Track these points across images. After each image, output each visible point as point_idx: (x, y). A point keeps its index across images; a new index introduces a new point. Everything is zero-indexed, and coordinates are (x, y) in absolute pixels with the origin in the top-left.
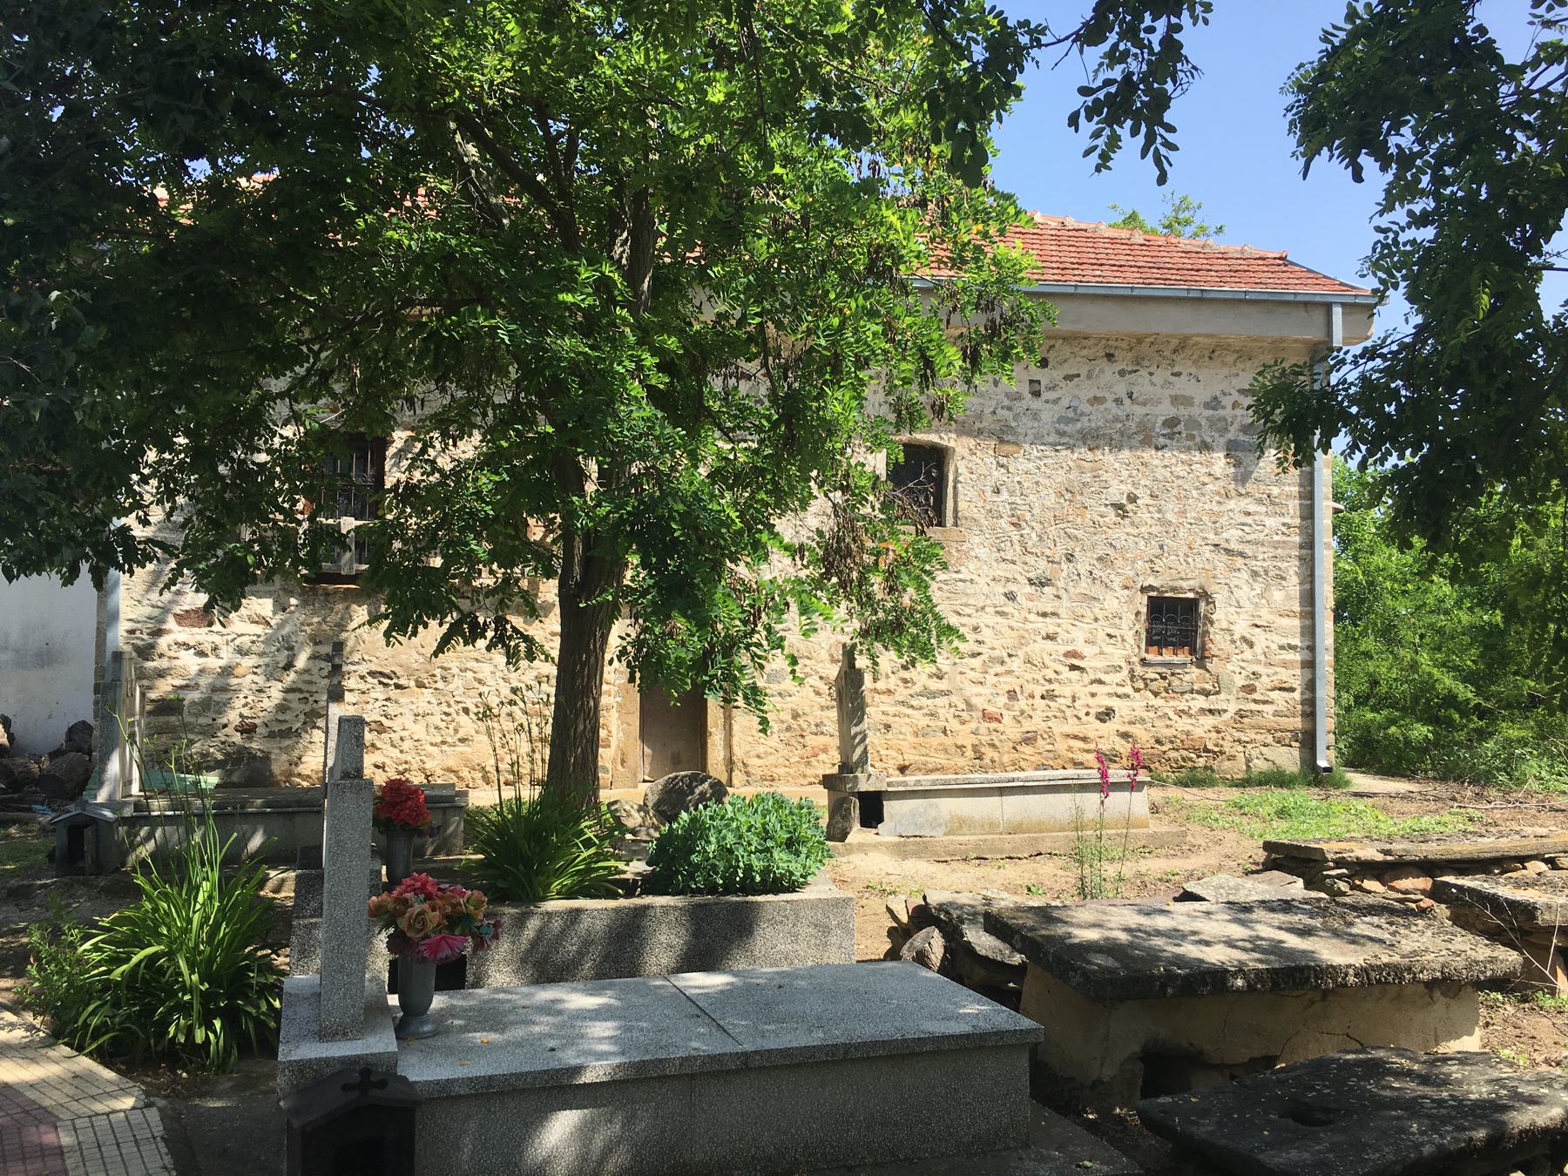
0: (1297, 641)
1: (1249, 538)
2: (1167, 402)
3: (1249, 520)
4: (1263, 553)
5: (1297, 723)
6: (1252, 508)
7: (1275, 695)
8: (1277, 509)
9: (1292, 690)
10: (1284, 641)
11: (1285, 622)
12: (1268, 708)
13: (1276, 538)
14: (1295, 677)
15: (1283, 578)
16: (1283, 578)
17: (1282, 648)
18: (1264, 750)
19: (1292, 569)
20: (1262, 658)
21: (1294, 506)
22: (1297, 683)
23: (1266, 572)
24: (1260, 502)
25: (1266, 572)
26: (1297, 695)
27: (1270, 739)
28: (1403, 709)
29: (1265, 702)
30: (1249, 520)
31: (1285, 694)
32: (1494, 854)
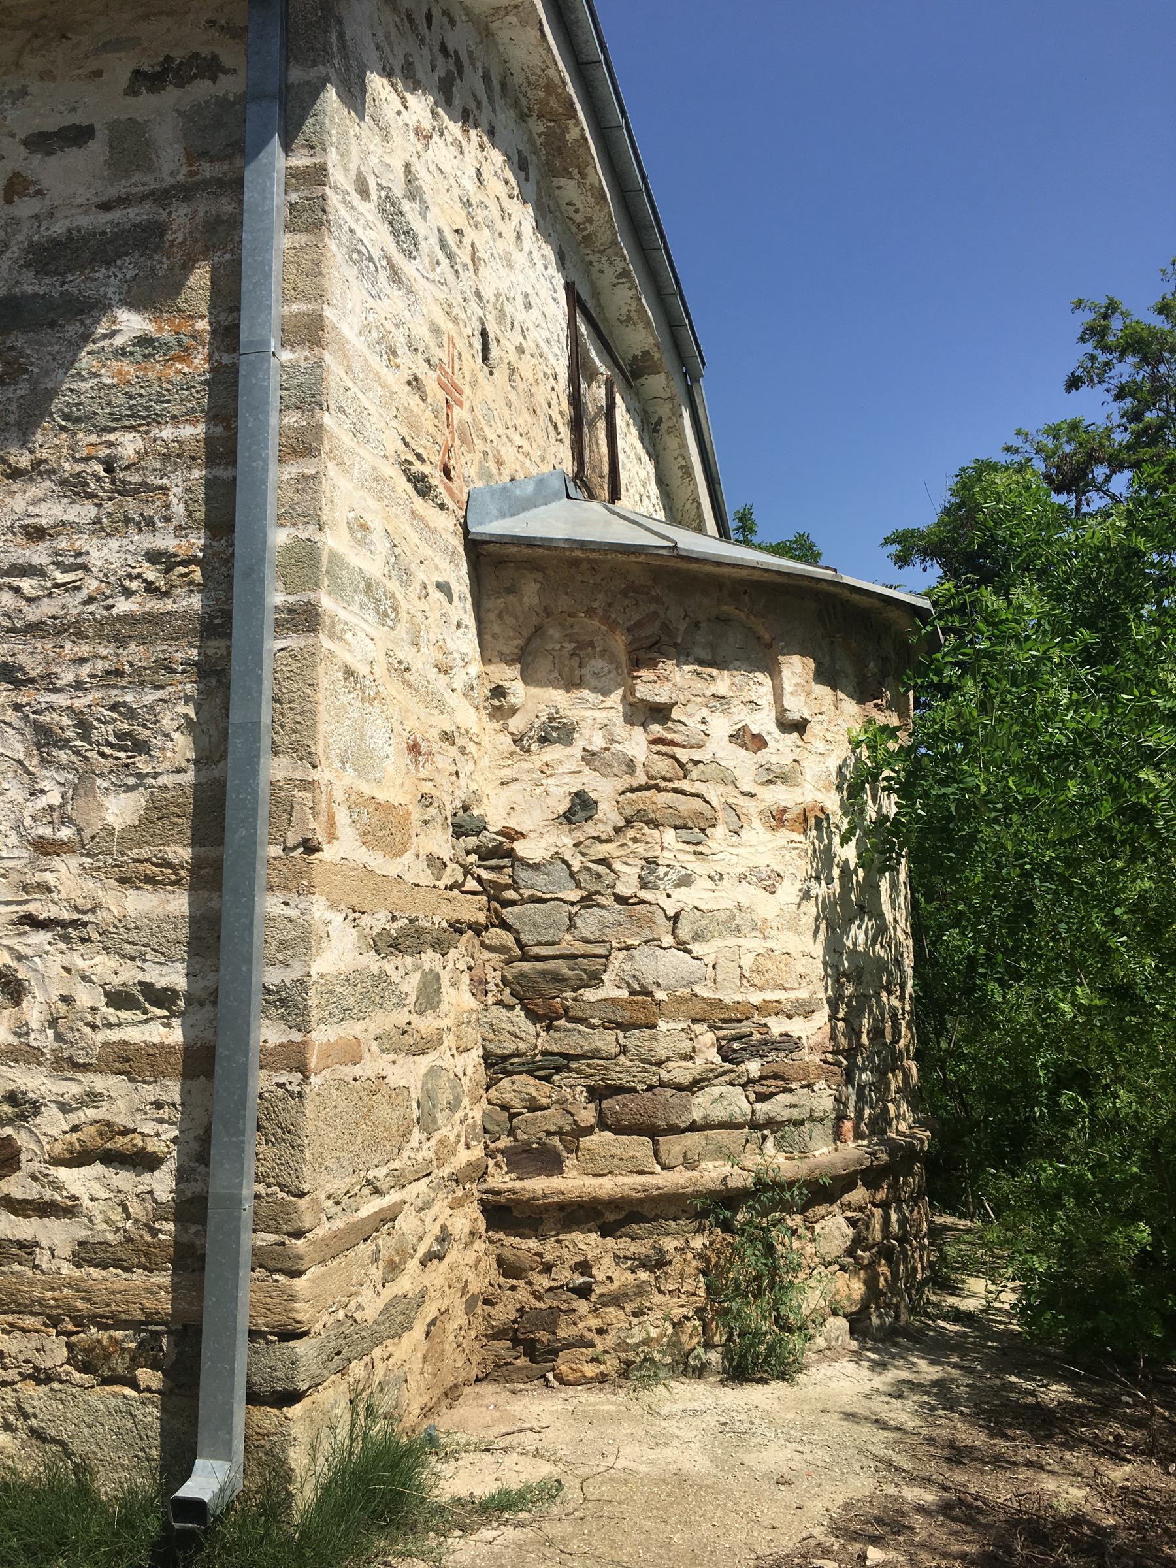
0: (174, 977)
1: (33, 614)
2: (406, 375)
3: (38, 555)
4: (72, 662)
5: (154, 1288)
6: (51, 513)
7: (79, 1182)
8: (131, 506)
9: (145, 1162)
10: (129, 974)
11: (141, 904)
12: (56, 1235)
13: (123, 606)
14: (146, 1110)
15: (141, 747)
16: (141, 747)
17: (119, 999)
18: (32, 1392)
19: (172, 714)
20: (44, 1040)
21: (182, 488)
22: (161, 1136)
23: (84, 728)
24: (76, 488)
25: (84, 728)
26: (162, 1183)
27: (56, 1354)
28: (1103, 1556)
29: (46, 1209)
30: (38, 555)
31: (124, 1179)
32: (206, 1365)
